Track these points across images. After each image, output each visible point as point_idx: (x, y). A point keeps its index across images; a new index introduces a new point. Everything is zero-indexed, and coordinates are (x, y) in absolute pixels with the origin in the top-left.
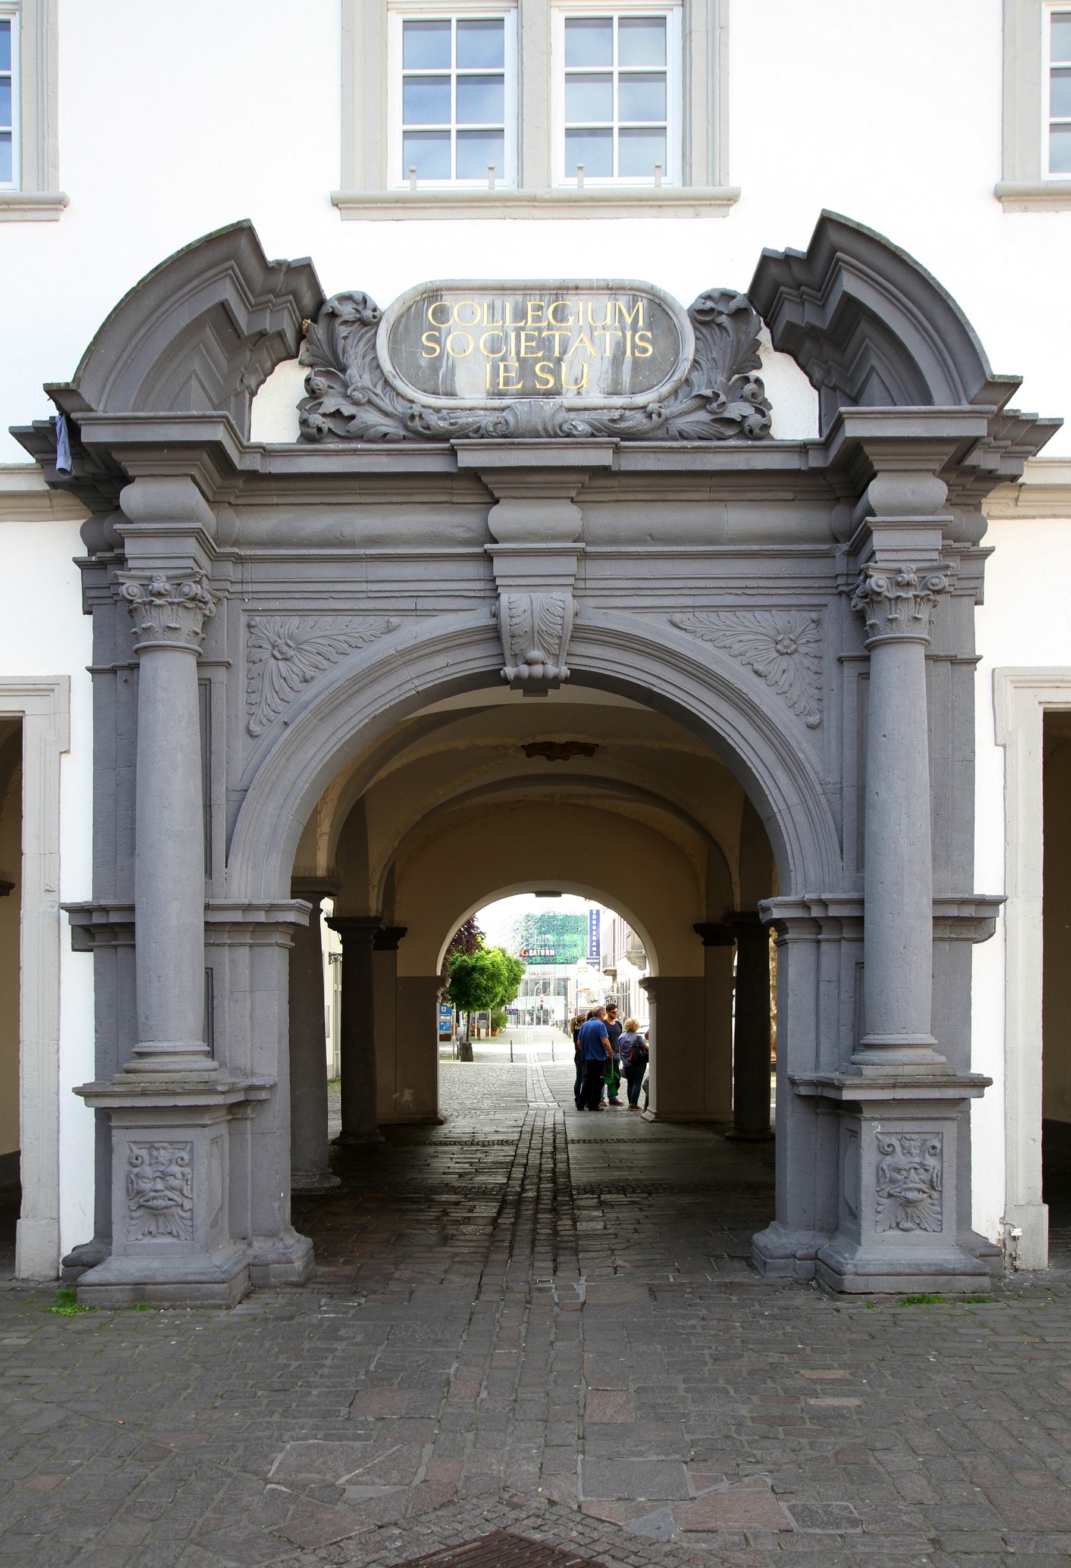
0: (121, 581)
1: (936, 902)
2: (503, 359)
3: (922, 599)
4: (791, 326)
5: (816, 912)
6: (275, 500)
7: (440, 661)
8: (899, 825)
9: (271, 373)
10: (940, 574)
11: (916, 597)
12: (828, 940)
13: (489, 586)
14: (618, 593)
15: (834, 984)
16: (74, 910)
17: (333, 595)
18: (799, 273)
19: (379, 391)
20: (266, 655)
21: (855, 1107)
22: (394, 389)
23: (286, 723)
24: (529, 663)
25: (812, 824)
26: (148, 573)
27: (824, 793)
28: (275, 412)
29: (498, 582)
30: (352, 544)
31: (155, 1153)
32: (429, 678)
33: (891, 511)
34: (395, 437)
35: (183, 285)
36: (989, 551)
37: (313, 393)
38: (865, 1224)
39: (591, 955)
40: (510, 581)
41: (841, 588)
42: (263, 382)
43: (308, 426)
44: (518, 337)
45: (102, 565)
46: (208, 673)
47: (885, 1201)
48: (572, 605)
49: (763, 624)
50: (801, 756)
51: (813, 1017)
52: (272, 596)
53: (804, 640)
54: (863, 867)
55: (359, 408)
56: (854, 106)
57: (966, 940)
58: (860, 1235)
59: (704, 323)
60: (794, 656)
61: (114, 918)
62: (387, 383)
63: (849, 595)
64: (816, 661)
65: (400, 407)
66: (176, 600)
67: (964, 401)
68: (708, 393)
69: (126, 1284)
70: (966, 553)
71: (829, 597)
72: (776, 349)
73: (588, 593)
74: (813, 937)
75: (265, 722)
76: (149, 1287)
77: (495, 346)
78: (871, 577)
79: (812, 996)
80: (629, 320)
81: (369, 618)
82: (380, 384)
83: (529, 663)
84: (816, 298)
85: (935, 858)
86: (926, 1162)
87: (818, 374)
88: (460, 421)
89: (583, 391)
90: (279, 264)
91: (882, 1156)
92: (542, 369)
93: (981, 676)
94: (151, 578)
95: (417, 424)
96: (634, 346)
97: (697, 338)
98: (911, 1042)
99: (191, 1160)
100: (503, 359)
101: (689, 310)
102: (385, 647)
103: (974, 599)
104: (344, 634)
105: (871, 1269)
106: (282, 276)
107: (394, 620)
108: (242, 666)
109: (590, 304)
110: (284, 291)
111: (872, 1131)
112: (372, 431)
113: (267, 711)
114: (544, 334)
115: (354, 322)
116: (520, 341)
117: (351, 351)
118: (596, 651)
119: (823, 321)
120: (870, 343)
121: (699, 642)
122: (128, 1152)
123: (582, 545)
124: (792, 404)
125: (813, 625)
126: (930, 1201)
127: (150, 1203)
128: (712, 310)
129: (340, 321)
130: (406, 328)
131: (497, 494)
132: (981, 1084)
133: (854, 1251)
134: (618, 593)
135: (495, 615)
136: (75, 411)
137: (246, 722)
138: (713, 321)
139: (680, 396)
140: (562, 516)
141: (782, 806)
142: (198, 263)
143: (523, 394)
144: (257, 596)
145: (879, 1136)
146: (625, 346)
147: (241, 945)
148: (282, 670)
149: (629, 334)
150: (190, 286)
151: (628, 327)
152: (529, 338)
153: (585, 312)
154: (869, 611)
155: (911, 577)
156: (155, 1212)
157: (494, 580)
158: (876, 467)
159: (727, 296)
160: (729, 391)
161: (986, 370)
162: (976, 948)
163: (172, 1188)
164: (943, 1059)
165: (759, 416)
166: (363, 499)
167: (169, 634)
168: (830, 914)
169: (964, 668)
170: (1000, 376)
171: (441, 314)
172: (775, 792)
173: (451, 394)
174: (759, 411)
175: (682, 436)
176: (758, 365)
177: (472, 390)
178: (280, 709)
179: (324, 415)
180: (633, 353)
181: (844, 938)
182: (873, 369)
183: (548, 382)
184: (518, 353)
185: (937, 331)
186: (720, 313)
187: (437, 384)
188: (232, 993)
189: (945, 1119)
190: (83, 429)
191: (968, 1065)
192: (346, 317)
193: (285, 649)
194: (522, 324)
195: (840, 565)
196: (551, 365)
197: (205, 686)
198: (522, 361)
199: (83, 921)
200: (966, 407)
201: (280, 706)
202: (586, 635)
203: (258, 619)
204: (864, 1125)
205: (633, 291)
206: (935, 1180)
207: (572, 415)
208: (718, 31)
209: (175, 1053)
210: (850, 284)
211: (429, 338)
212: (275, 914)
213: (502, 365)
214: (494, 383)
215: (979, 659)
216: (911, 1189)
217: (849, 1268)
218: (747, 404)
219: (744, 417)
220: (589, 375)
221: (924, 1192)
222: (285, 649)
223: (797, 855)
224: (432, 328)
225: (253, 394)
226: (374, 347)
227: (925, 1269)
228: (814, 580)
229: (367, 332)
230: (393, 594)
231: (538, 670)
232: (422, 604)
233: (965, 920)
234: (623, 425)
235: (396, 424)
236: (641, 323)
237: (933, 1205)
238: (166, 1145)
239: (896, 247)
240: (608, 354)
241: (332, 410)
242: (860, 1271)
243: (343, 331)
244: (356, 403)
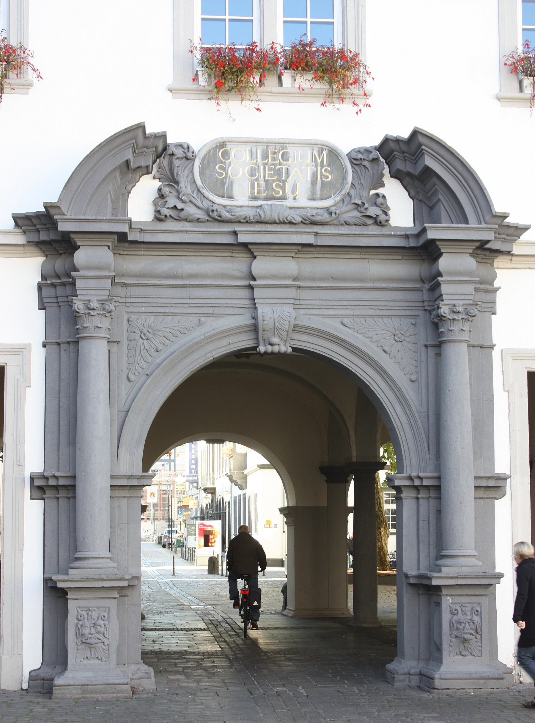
0: (74, 302)
1: (475, 478)
2: (257, 180)
3: (465, 319)
4: (399, 171)
5: (417, 483)
6: (143, 253)
7: (225, 342)
8: (457, 438)
9: (138, 182)
10: (474, 308)
11: (462, 319)
12: (423, 498)
13: (251, 302)
14: (316, 307)
15: (426, 522)
16: (410, 474)
18: (403, 147)
19: (195, 196)
20: (137, 337)
21: (438, 588)
22: (202, 194)
24: (271, 344)
25: (414, 434)
26: (87, 298)
28: (141, 202)
29: (256, 301)
30: (182, 277)
31: (90, 613)
32: (219, 350)
33: (450, 273)
34: (203, 220)
35: (111, 151)
36: (498, 289)
38: (445, 653)
39: (190, 472)
41: (426, 308)
42: (134, 186)
43: (160, 214)
44: (264, 168)
47: (453, 640)
48: (294, 314)
49: (388, 325)
51: (416, 540)
52: (141, 304)
53: (408, 334)
54: (439, 458)
55: (185, 205)
56: (428, 71)
57: (491, 498)
58: (442, 658)
60: (404, 343)
62: (199, 190)
63: (430, 312)
64: (414, 345)
65: (206, 204)
66: (101, 313)
67: (483, 223)
68: (359, 202)
69: (78, 685)
70: (487, 288)
71: (420, 312)
72: (391, 177)
73: (301, 307)
74: (415, 495)
75: (137, 373)
76: (89, 687)
77: (253, 172)
78: (441, 308)
79: (415, 528)
80: (319, 161)
81: (189, 318)
83: (271, 344)
84: (412, 160)
85: (475, 453)
86: (473, 619)
87: (412, 193)
88: (237, 214)
89: (297, 198)
90: (151, 135)
91: (452, 615)
92: (276, 186)
93: (496, 354)
95: (215, 215)
96: (322, 175)
98: (464, 554)
99: (109, 617)
100: (257, 180)
102: (198, 334)
103: (491, 313)
104: (178, 326)
105: (448, 676)
106: (152, 139)
107: (203, 319)
108: (125, 342)
110: (151, 146)
111: (447, 601)
113: (137, 367)
114: (277, 167)
116: (265, 171)
118: (305, 338)
119: (417, 171)
120: (438, 188)
121: (356, 334)
122: (76, 613)
124: (400, 208)
125: (412, 326)
126: (476, 640)
127: (88, 641)
130: (208, 161)
131: (255, 254)
132: (500, 576)
133: (439, 667)
134: (316, 307)
135: (255, 318)
136: (56, 215)
137: (127, 373)
138: (361, 164)
139: (345, 202)
140: (288, 265)
141: (399, 424)
142: (118, 141)
143: (267, 198)
145: (450, 605)
146: (317, 175)
147: (124, 497)
148: (146, 345)
149: (319, 168)
150: (113, 152)
151: (319, 165)
153: (297, 155)
154: (440, 324)
155: (461, 309)
156: (90, 645)
157: (254, 299)
158: (442, 251)
161: (492, 209)
162: (496, 502)
163: (98, 632)
164: (480, 563)
165: (384, 216)
166: (187, 254)
167: (97, 330)
169: (487, 350)
170: (499, 213)
171: (226, 154)
172: (395, 415)
173: (231, 197)
176: (382, 185)
177: (241, 198)
178: (144, 366)
180: (321, 179)
181: (431, 497)
182: (439, 200)
183: (279, 192)
184: (264, 177)
185: (470, 187)
187: (223, 192)
188: (119, 524)
189: (482, 595)
190: (59, 224)
191: (494, 568)
193: (148, 334)
194: (266, 161)
195: (426, 297)
196: (281, 184)
198: (266, 181)
200: (484, 225)
201: (144, 365)
202: (299, 330)
203: (133, 317)
204: (443, 598)
206: (478, 628)
207: (292, 211)
208: (360, 8)
209: (99, 558)
210: (429, 162)
211: (220, 168)
212: (142, 480)
213: (256, 183)
215: (494, 345)
216: (466, 633)
217: (437, 676)
218: (378, 208)
220: (300, 194)
221: (473, 635)
222: (148, 334)
223: (407, 450)
224: (222, 162)
226: (192, 171)
227: (474, 676)
228: (414, 303)
229: (189, 164)
230: (202, 305)
231: (276, 349)
232: (217, 311)
233: (491, 487)
236: (325, 163)
237: (477, 642)
238: (96, 609)
239: (449, 147)
240: (309, 179)
241: (172, 206)
242: (443, 677)
243: (177, 163)
244: (184, 202)
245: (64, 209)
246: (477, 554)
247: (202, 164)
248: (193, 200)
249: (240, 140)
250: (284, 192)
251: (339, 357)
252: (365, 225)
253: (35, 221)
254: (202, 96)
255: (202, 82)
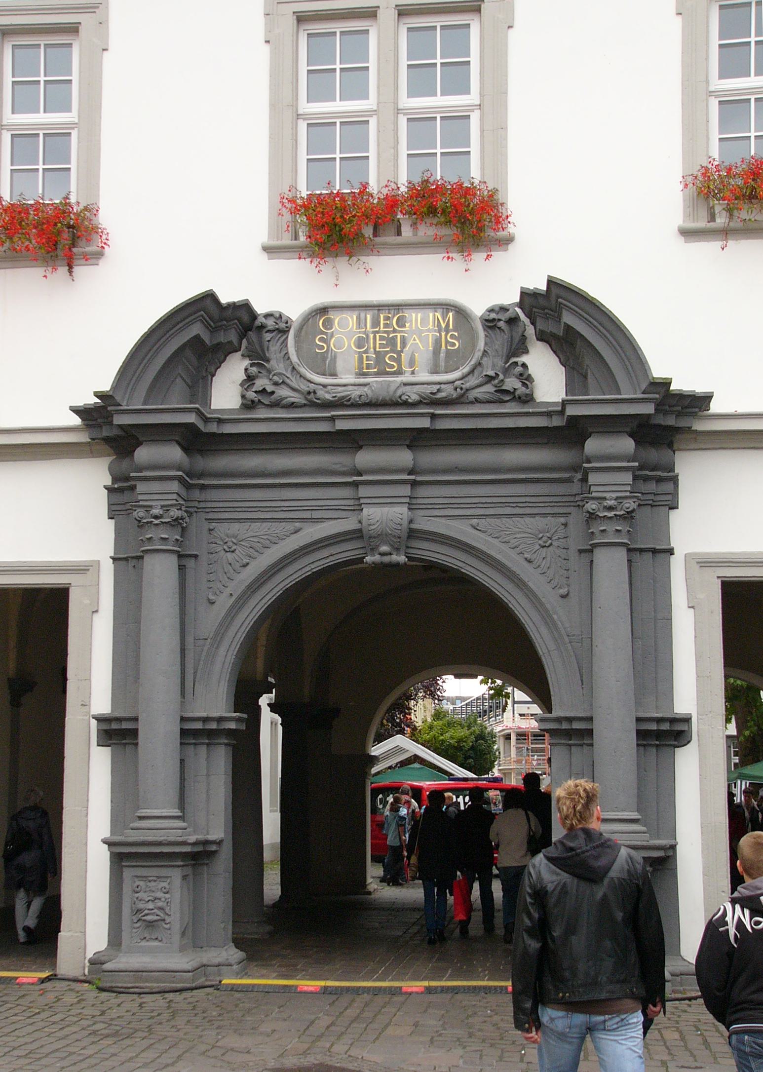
9: (223, 362)
14: (437, 506)
16: (100, 719)
17: (259, 509)
18: (542, 302)
22: (298, 373)
23: (231, 595)
27: (570, 642)
37: (250, 379)
40: (368, 501)
42: (219, 367)
45: (121, 490)
46: (184, 562)
50: (555, 617)
52: (223, 510)
59: (490, 327)
61: (125, 725)
65: (304, 387)
72: (538, 339)
75: (218, 593)
77: (360, 343)
80: (443, 326)
82: (290, 369)
94: (151, 507)
96: (447, 342)
97: (486, 336)
100: (366, 352)
101: (480, 318)
109: (419, 315)
112: (284, 401)
113: (220, 586)
115: (274, 331)
117: (272, 349)
121: (490, 539)
123: (412, 477)
125: (563, 527)
128: (494, 320)
129: (265, 330)
138: (495, 326)
143: (377, 374)
144: (213, 510)
149: (443, 334)
152: (381, 338)
159: (503, 309)
160: (506, 371)
168: (574, 727)
171: (328, 324)
173: (334, 375)
174: (524, 384)
175: (477, 401)
177: (346, 378)
179: (256, 392)
180: (446, 347)
184: (375, 348)
186: (500, 320)
192: (269, 328)
197: (182, 568)
199: (105, 727)
205: (445, 307)
210: (568, 318)
214: (360, 367)
219: (515, 389)
224: (323, 333)
225: (213, 375)
226: (286, 346)
233: (664, 735)
234: (439, 396)
235: (300, 396)
236: (451, 327)
241: (261, 389)
244: (276, 384)
245: (118, 398)
246: (640, 817)
247: (297, 335)
248: (287, 381)
249: (345, 304)
250: (400, 365)
251: (468, 568)
252: (502, 402)
253: (95, 415)
254: (292, 254)
255: (302, 239)
